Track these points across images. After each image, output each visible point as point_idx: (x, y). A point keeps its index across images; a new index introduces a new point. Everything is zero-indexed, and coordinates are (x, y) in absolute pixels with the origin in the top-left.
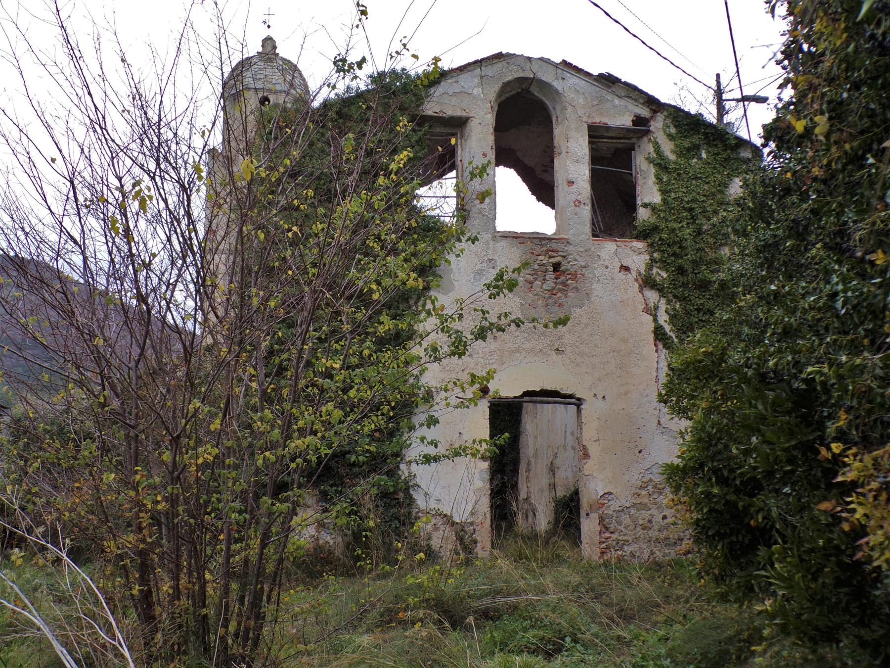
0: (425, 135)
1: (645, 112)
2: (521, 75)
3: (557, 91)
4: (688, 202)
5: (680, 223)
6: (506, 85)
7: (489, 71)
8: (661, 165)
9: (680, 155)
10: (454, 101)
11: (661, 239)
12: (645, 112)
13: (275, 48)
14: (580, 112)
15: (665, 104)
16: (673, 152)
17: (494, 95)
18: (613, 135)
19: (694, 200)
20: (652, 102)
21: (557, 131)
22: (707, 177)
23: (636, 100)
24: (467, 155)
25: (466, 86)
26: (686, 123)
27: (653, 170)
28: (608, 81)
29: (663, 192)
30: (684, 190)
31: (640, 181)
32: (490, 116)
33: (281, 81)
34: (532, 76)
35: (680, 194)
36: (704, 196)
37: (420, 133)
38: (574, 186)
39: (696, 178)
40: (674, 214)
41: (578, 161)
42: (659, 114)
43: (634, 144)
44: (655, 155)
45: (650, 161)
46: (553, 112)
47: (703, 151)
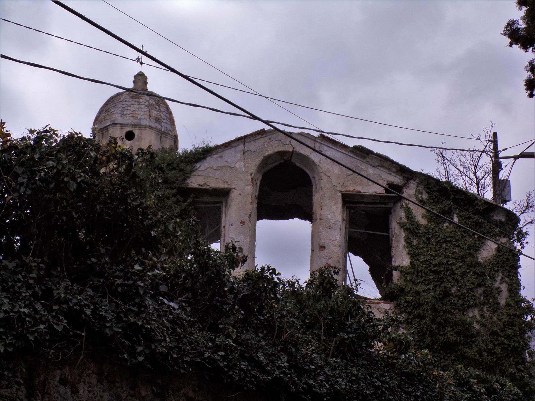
0: (189, 205)
1: (397, 180)
2: (281, 149)
3: (314, 163)
4: (436, 265)
5: (427, 285)
6: (267, 160)
7: (251, 146)
8: (412, 229)
9: (430, 220)
10: (218, 174)
11: (406, 301)
12: (397, 180)
13: (146, 83)
14: (335, 182)
15: (416, 173)
16: (424, 216)
17: (255, 168)
18: (369, 200)
19: (440, 264)
20: (403, 170)
21: (316, 198)
22: (457, 240)
23: (389, 169)
24: (228, 222)
25: (229, 161)
26: (440, 192)
27: (403, 235)
28: (361, 152)
29: (412, 255)
30: (433, 254)
31: (394, 244)
32: (249, 187)
33: (146, 116)
34: (291, 150)
35: (428, 258)
36: (454, 258)
37: (184, 205)
38: (326, 251)
39: (446, 242)
40: (422, 277)
41: (330, 227)
42: (412, 181)
43: (391, 208)
44: (406, 220)
45: (402, 225)
46: (313, 181)
47: (455, 216)
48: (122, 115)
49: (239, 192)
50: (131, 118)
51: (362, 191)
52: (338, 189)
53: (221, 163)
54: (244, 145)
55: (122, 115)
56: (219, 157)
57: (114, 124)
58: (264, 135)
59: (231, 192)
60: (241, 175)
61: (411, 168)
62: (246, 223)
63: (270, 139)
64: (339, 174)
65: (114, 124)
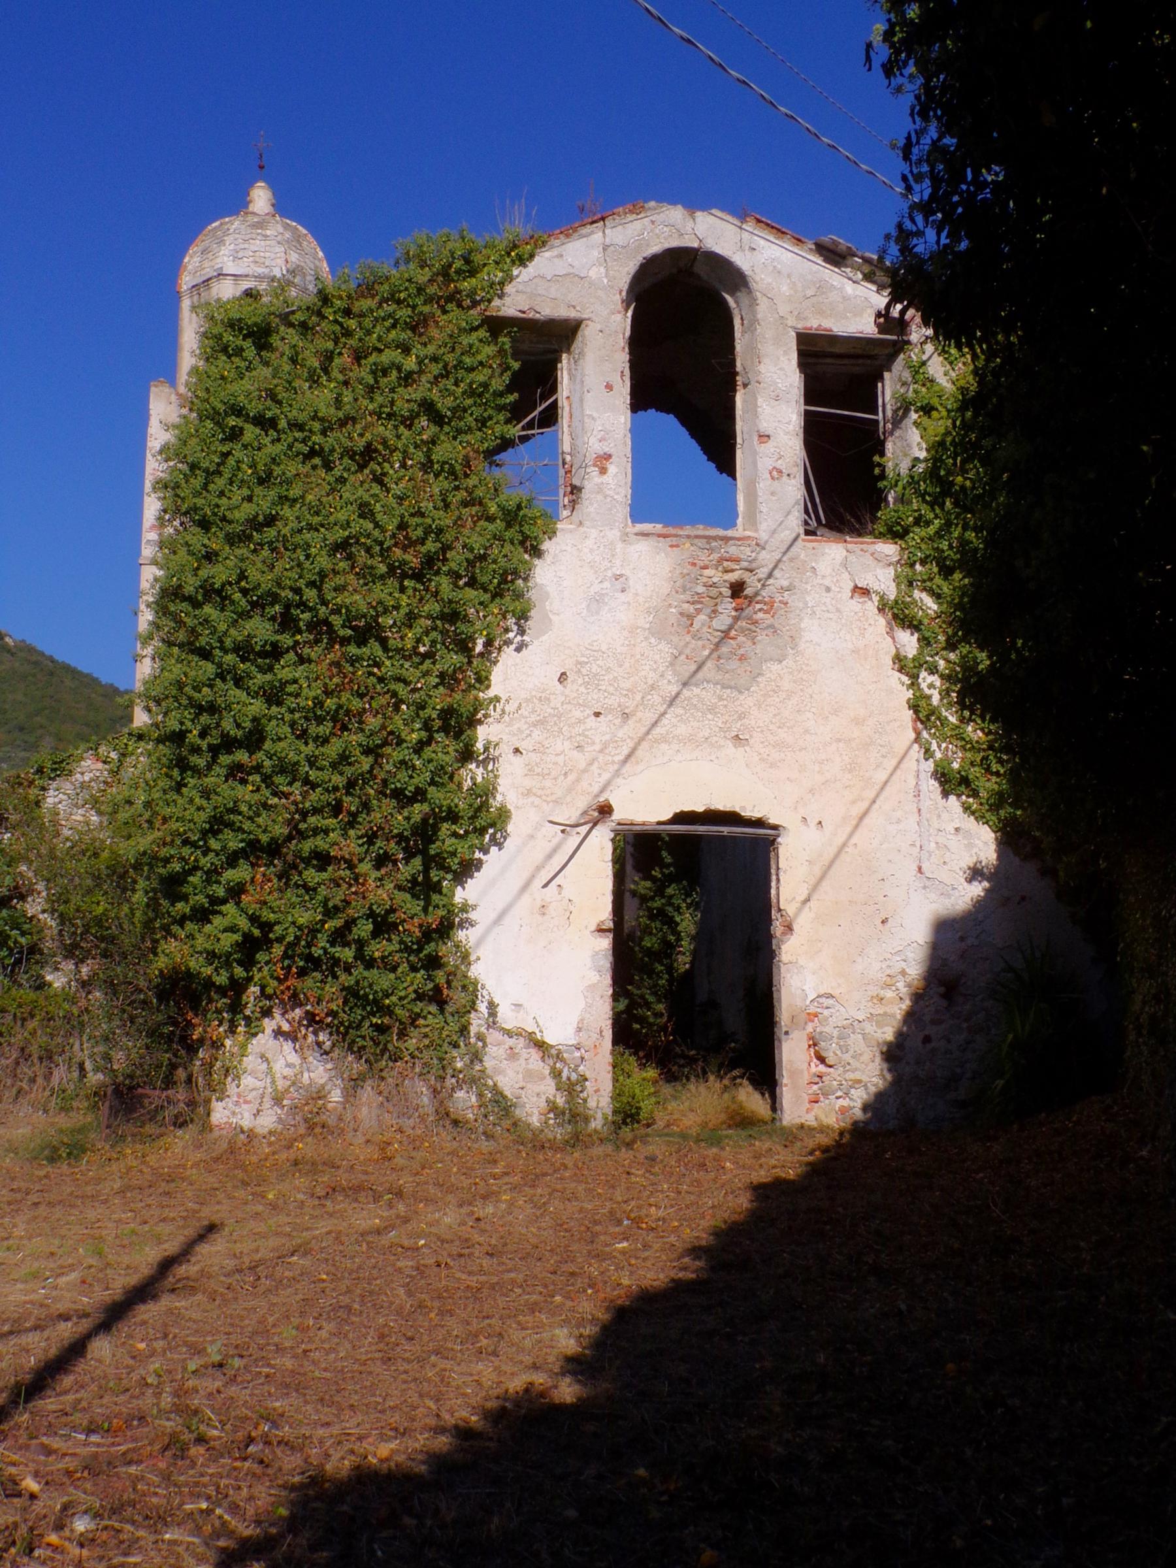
14: (783, 309)
32: (619, 317)
38: (771, 444)
48: (236, 258)
49: (599, 327)
50: (252, 265)
51: (835, 329)
52: (790, 323)
53: (560, 268)
54: (604, 232)
55: (236, 258)
56: (557, 256)
57: (221, 275)
58: (642, 215)
59: (583, 326)
60: (600, 293)
61: (683, 432)
62: (615, 388)
63: (653, 222)
64: (790, 295)
65: (221, 275)
